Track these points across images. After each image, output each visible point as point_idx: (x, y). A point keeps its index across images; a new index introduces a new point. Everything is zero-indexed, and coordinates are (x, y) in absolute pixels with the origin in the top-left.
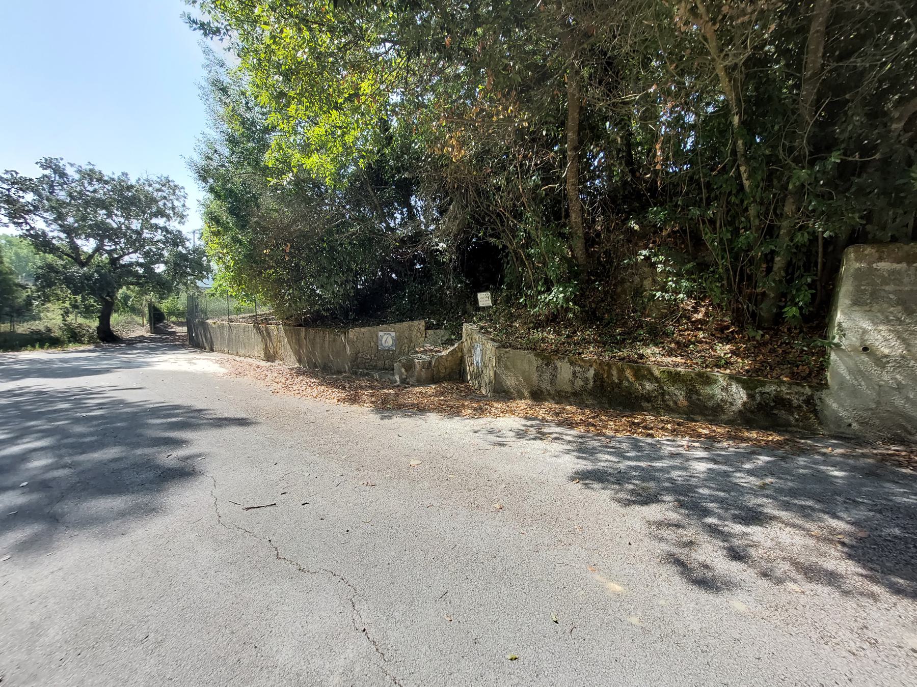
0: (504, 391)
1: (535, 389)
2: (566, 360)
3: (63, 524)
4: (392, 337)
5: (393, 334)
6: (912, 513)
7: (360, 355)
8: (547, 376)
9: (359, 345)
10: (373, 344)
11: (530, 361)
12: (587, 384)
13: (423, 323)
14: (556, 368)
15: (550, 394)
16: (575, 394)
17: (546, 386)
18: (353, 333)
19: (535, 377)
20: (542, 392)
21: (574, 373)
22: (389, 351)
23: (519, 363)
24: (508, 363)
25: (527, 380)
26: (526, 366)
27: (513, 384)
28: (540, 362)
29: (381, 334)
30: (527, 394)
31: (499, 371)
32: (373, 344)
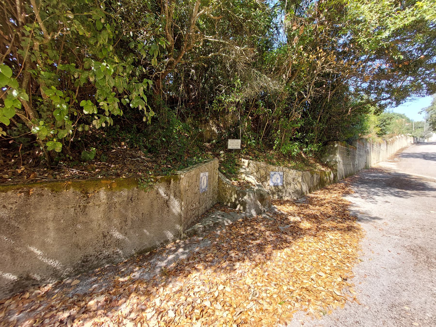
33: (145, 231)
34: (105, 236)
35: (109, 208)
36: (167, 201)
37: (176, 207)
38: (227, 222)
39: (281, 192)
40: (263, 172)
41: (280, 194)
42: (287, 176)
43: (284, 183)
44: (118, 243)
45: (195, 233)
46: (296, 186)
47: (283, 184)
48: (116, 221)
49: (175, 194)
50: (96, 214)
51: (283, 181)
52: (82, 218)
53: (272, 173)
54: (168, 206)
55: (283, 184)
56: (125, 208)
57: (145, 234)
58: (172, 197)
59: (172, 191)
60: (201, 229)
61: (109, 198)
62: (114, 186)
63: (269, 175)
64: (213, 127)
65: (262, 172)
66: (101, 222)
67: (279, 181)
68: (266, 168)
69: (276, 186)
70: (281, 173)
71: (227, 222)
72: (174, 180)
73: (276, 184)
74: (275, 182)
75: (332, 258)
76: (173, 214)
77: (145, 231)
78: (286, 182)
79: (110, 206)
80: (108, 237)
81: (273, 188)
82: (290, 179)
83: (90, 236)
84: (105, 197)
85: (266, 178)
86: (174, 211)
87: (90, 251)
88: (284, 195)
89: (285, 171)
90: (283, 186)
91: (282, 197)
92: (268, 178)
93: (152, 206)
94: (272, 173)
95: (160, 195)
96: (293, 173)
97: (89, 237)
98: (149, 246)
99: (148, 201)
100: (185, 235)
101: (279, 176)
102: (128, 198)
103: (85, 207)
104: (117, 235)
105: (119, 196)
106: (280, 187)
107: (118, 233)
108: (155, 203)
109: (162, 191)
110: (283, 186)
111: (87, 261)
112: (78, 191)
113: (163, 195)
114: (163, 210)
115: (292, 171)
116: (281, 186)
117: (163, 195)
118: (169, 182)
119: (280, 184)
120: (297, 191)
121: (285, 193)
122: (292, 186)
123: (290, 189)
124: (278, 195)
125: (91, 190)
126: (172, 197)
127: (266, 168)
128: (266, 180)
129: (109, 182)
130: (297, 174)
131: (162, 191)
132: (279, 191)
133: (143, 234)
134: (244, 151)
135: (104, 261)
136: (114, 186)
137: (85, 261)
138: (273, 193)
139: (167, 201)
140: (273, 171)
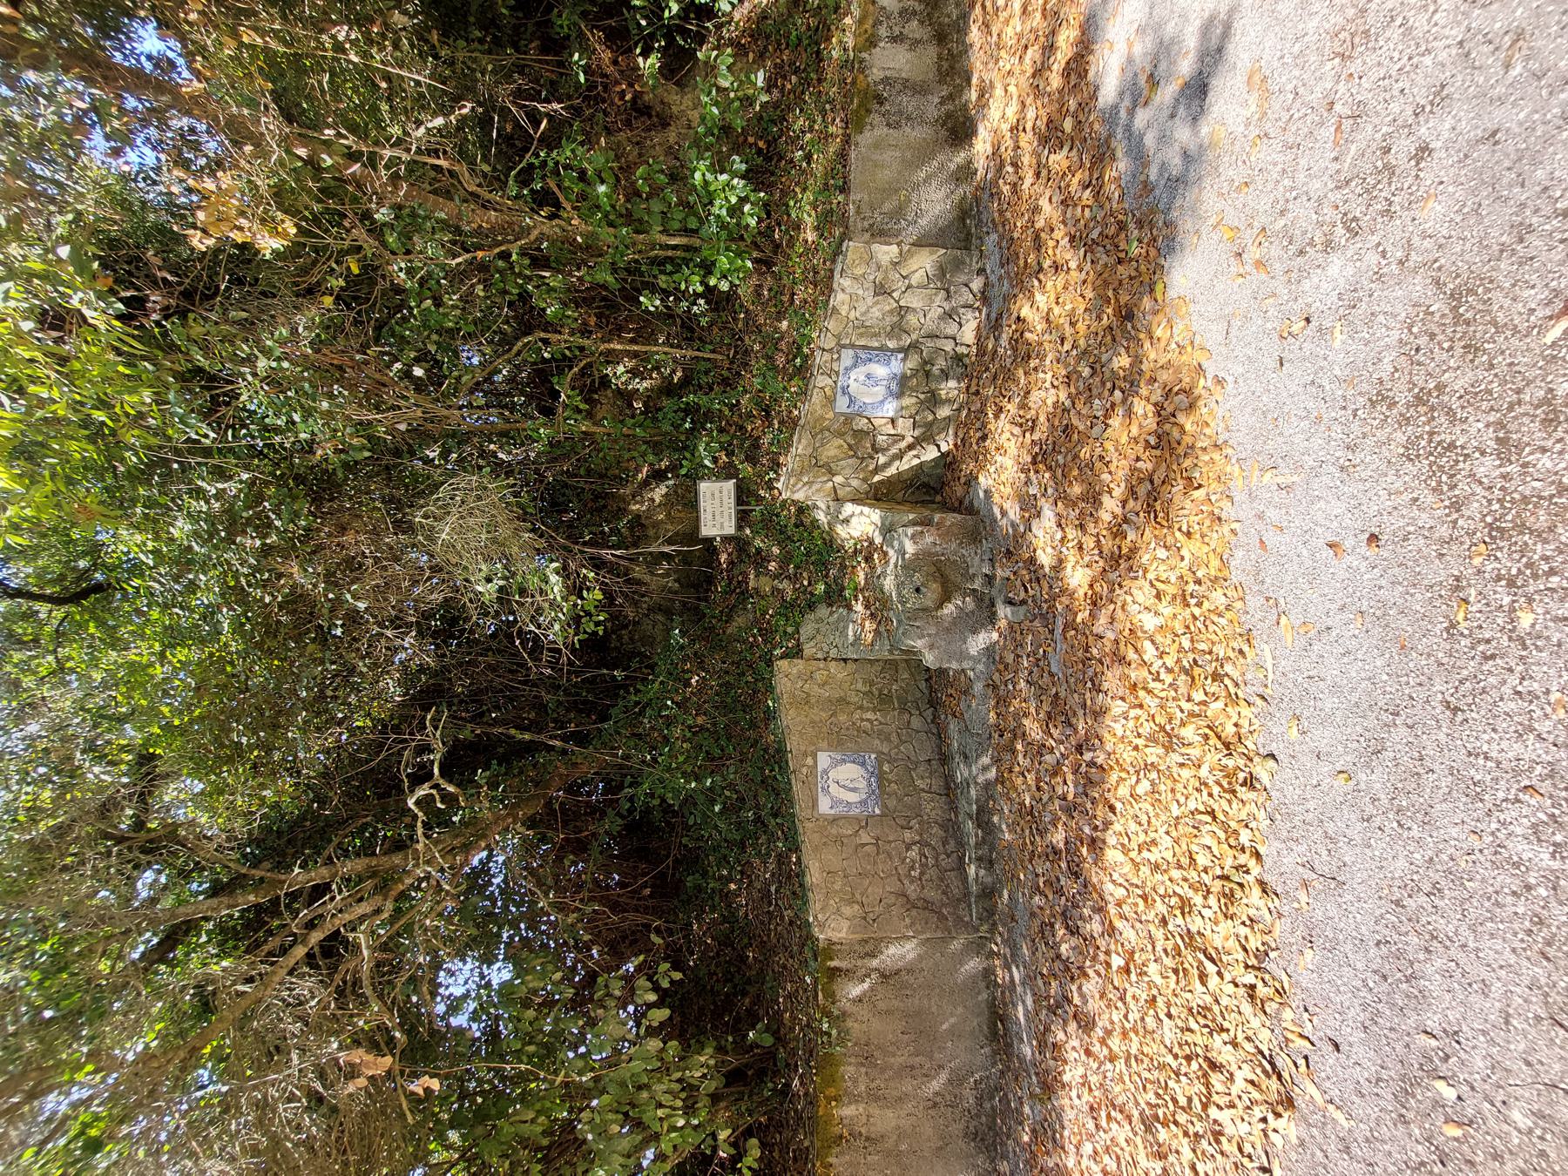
0: (964, 220)
1: (943, 133)
2: (864, 55)
3: (1177, 183)
4: (836, 764)
5: (824, 759)
6: (1519, 4)
7: (912, 890)
8: (909, 103)
9: (875, 891)
10: (865, 838)
11: (877, 145)
12: (914, 13)
13: (783, 664)
14: (886, 81)
15: (951, 97)
16: (941, 38)
17: (932, 107)
18: (832, 924)
19: (916, 134)
20: (949, 115)
21: (894, 39)
22: (881, 777)
23: (885, 175)
24: (887, 207)
25: (923, 154)
26: (888, 156)
27: (941, 194)
28: (875, 118)
29: (824, 806)
30: (960, 158)
31: (912, 233)
32: (865, 838)
33: (944, 1027)
34: (935, 1105)
35: (877, 1099)
36: (883, 976)
37: (901, 952)
38: (985, 769)
39: (931, 362)
40: (832, 449)
41: (941, 363)
42: (863, 328)
43: (891, 344)
44: (956, 1080)
45: (989, 893)
46: (915, 280)
47: (900, 350)
48: (907, 1086)
49: (867, 954)
50: (885, 1120)
51: (880, 349)
52: (889, 1143)
53: (842, 404)
54: (897, 972)
55: (900, 350)
56: (883, 1070)
57: (953, 1026)
58: (875, 963)
59: (859, 963)
60: (982, 872)
61: (855, 1099)
62: (832, 1091)
63: (848, 419)
64: (653, 500)
65: (832, 452)
66: (903, 1113)
67: (881, 371)
68: (820, 431)
69: (902, 385)
70: (847, 356)
71: (985, 769)
72: (832, 959)
73: (894, 386)
74: (880, 391)
75: (1227, 745)
76: (920, 958)
77: (944, 1027)
78: (890, 335)
79: (874, 1097)
80: (938, 1099)
81: (908, 401)
82: (878, 312)
83: (928, 1130)
84: (853, 1107)
85: (860, 434)
86: (911, 956)
87: (957, 1128)
88: (948, 346)
89: (838, 337)
90: (906, 351)
91: (958, 358)
92: (862, 424)
93: (888, 1012)
94: (842, 404)
95: (864, 993)
96: (851, 296)
97: (930, 1132)
98: (984, 1019)
99: (876, 1024)
100: (985, 927)
101: (858, 374)
102: (863, 1065)
103: (867, 1139)
104: (935, 1085)
105: (855, 1081)
106: (913, 362)
107: (934, 1083)
108: (882, 1005)
109: (856, 990)
110: (906, 351)
111: (976, 1134)
112: (836, 1150)
113: (866, 985)
114: (904, 986)
115: (840, 296)
116: (904, 360)
117: (866, 985)
118: (834, 973)
119: (897, 366)
120: (942, 271)
121: (940, 343)
122: (913, 301)
123: (925, 309)
124: (945, 375)
125: (837, 1130)
126: (875, 963)
127: (820, 431)
128: (871, 433)
129: (823, 1102)
130: (859, 271)
131: (856, 990)
132: (924, 371)
133: (951, 1032)
134: (746, 469)
135: (987, 1105)
136: (832, 1091)
137: (974, 1136)
138: (933, 400)
139: (883, 976)
140: (830, 401)
